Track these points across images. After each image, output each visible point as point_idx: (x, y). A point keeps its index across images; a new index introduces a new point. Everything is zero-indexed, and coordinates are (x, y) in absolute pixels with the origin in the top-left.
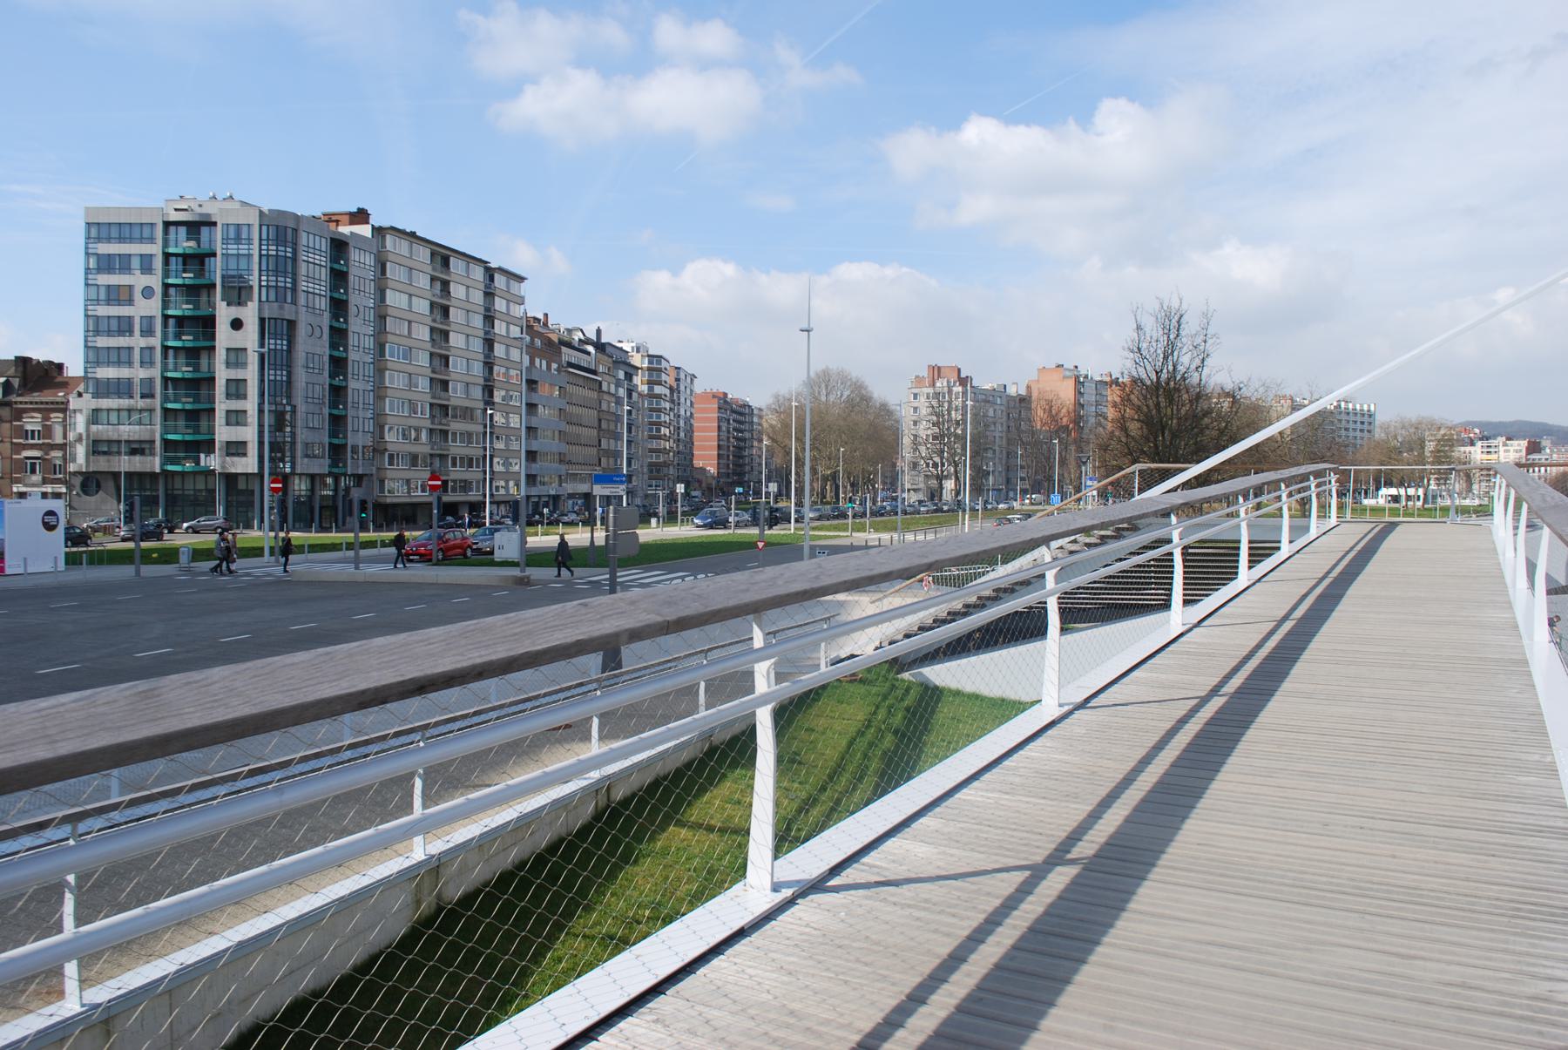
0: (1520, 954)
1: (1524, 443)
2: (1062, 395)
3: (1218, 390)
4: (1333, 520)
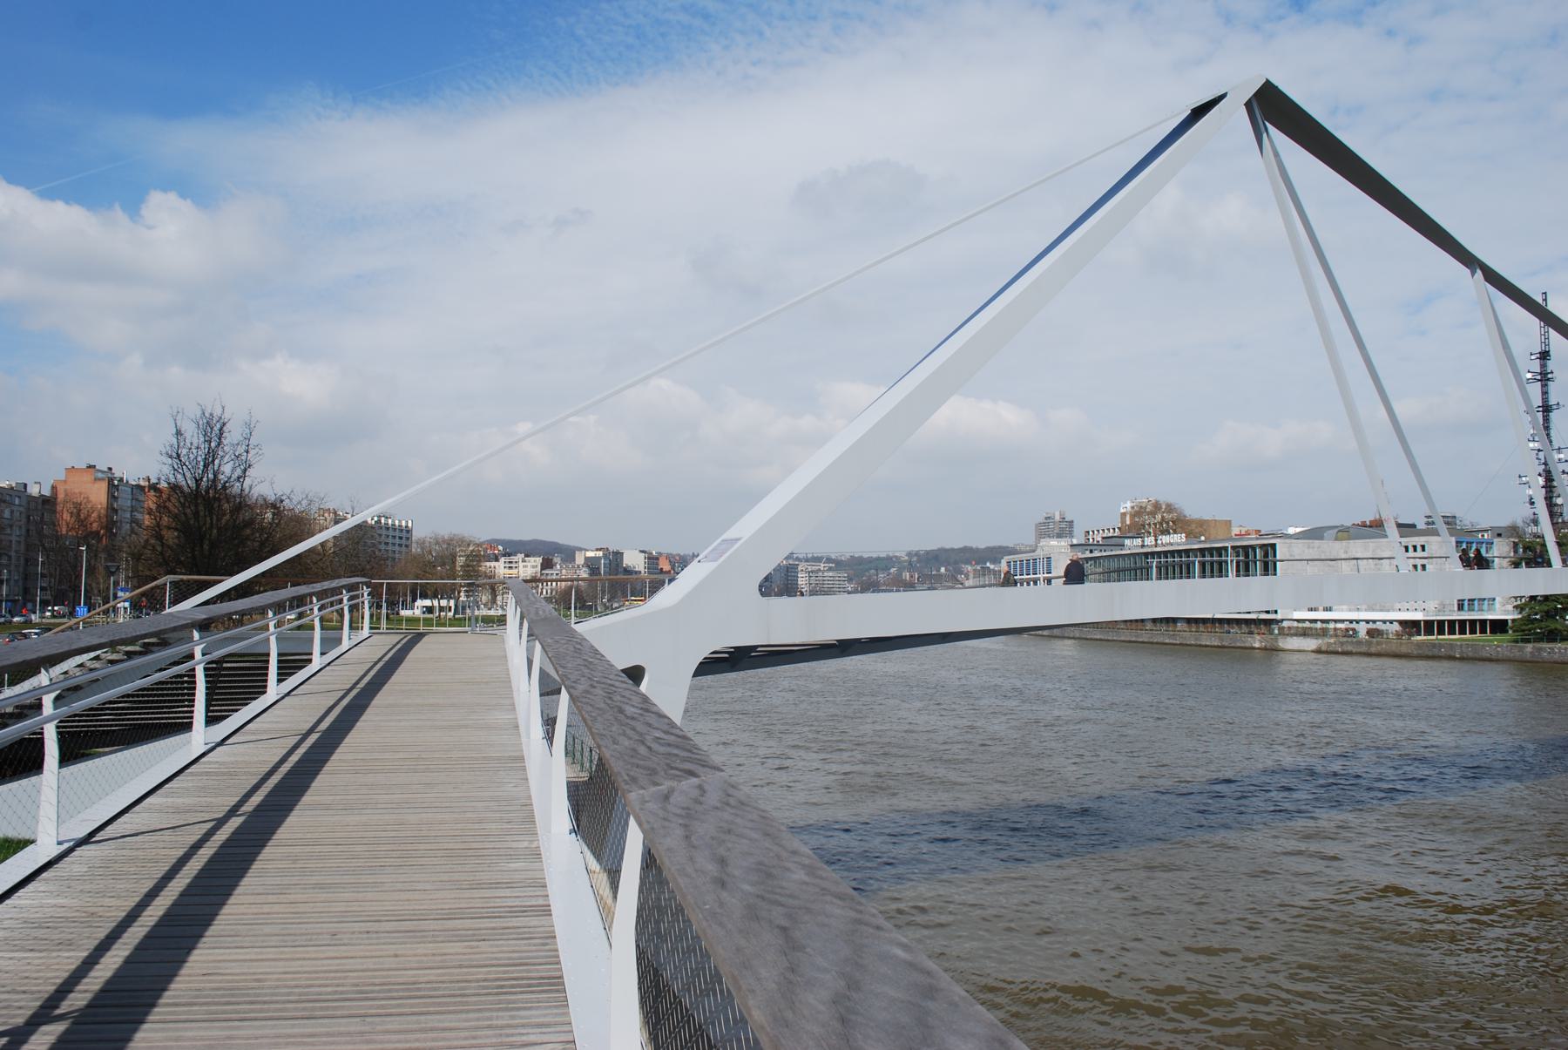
0: (502, 1027)
1: (539, 560)
2: (93, 498)
3: (261, 501)
4: (366, 632)
